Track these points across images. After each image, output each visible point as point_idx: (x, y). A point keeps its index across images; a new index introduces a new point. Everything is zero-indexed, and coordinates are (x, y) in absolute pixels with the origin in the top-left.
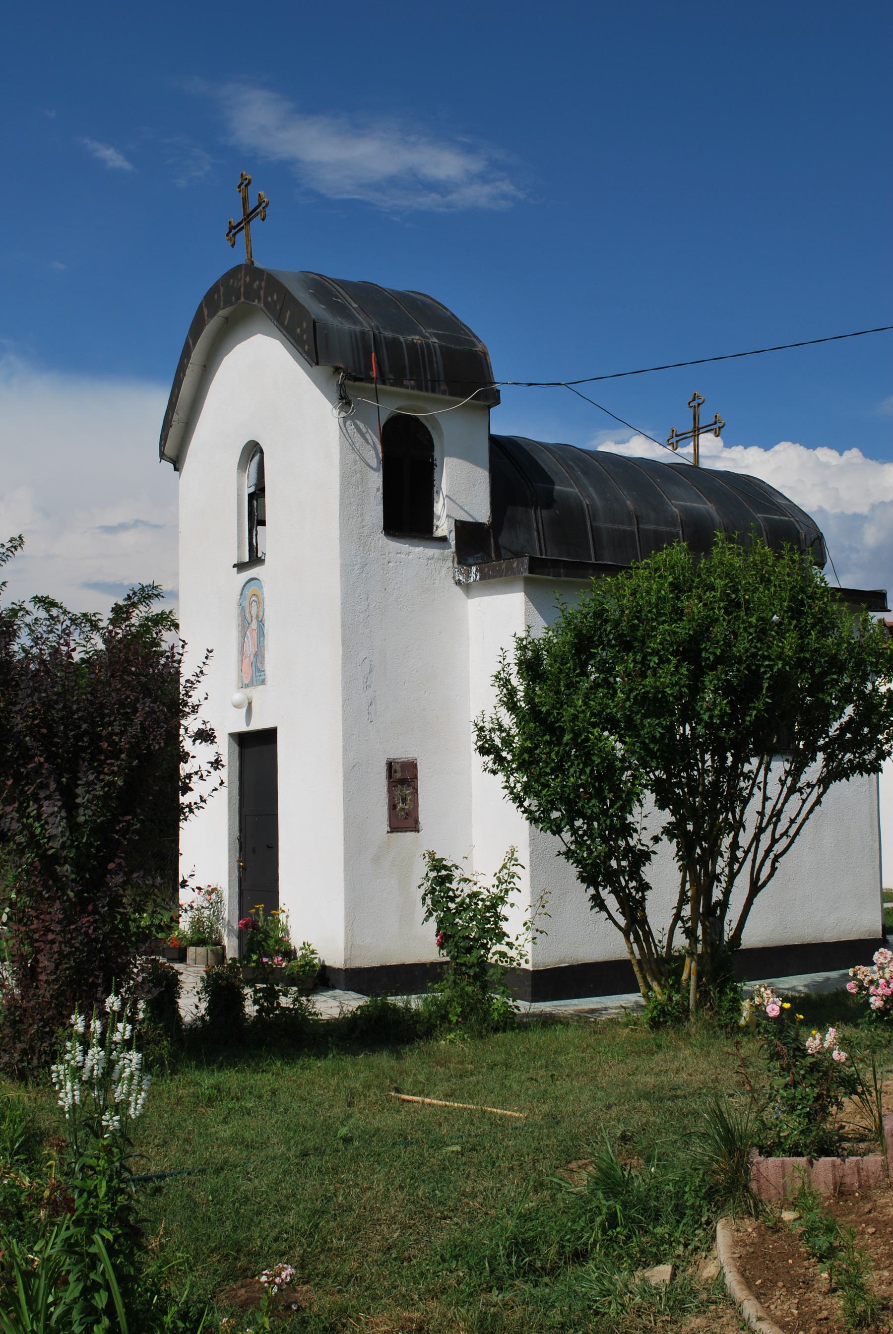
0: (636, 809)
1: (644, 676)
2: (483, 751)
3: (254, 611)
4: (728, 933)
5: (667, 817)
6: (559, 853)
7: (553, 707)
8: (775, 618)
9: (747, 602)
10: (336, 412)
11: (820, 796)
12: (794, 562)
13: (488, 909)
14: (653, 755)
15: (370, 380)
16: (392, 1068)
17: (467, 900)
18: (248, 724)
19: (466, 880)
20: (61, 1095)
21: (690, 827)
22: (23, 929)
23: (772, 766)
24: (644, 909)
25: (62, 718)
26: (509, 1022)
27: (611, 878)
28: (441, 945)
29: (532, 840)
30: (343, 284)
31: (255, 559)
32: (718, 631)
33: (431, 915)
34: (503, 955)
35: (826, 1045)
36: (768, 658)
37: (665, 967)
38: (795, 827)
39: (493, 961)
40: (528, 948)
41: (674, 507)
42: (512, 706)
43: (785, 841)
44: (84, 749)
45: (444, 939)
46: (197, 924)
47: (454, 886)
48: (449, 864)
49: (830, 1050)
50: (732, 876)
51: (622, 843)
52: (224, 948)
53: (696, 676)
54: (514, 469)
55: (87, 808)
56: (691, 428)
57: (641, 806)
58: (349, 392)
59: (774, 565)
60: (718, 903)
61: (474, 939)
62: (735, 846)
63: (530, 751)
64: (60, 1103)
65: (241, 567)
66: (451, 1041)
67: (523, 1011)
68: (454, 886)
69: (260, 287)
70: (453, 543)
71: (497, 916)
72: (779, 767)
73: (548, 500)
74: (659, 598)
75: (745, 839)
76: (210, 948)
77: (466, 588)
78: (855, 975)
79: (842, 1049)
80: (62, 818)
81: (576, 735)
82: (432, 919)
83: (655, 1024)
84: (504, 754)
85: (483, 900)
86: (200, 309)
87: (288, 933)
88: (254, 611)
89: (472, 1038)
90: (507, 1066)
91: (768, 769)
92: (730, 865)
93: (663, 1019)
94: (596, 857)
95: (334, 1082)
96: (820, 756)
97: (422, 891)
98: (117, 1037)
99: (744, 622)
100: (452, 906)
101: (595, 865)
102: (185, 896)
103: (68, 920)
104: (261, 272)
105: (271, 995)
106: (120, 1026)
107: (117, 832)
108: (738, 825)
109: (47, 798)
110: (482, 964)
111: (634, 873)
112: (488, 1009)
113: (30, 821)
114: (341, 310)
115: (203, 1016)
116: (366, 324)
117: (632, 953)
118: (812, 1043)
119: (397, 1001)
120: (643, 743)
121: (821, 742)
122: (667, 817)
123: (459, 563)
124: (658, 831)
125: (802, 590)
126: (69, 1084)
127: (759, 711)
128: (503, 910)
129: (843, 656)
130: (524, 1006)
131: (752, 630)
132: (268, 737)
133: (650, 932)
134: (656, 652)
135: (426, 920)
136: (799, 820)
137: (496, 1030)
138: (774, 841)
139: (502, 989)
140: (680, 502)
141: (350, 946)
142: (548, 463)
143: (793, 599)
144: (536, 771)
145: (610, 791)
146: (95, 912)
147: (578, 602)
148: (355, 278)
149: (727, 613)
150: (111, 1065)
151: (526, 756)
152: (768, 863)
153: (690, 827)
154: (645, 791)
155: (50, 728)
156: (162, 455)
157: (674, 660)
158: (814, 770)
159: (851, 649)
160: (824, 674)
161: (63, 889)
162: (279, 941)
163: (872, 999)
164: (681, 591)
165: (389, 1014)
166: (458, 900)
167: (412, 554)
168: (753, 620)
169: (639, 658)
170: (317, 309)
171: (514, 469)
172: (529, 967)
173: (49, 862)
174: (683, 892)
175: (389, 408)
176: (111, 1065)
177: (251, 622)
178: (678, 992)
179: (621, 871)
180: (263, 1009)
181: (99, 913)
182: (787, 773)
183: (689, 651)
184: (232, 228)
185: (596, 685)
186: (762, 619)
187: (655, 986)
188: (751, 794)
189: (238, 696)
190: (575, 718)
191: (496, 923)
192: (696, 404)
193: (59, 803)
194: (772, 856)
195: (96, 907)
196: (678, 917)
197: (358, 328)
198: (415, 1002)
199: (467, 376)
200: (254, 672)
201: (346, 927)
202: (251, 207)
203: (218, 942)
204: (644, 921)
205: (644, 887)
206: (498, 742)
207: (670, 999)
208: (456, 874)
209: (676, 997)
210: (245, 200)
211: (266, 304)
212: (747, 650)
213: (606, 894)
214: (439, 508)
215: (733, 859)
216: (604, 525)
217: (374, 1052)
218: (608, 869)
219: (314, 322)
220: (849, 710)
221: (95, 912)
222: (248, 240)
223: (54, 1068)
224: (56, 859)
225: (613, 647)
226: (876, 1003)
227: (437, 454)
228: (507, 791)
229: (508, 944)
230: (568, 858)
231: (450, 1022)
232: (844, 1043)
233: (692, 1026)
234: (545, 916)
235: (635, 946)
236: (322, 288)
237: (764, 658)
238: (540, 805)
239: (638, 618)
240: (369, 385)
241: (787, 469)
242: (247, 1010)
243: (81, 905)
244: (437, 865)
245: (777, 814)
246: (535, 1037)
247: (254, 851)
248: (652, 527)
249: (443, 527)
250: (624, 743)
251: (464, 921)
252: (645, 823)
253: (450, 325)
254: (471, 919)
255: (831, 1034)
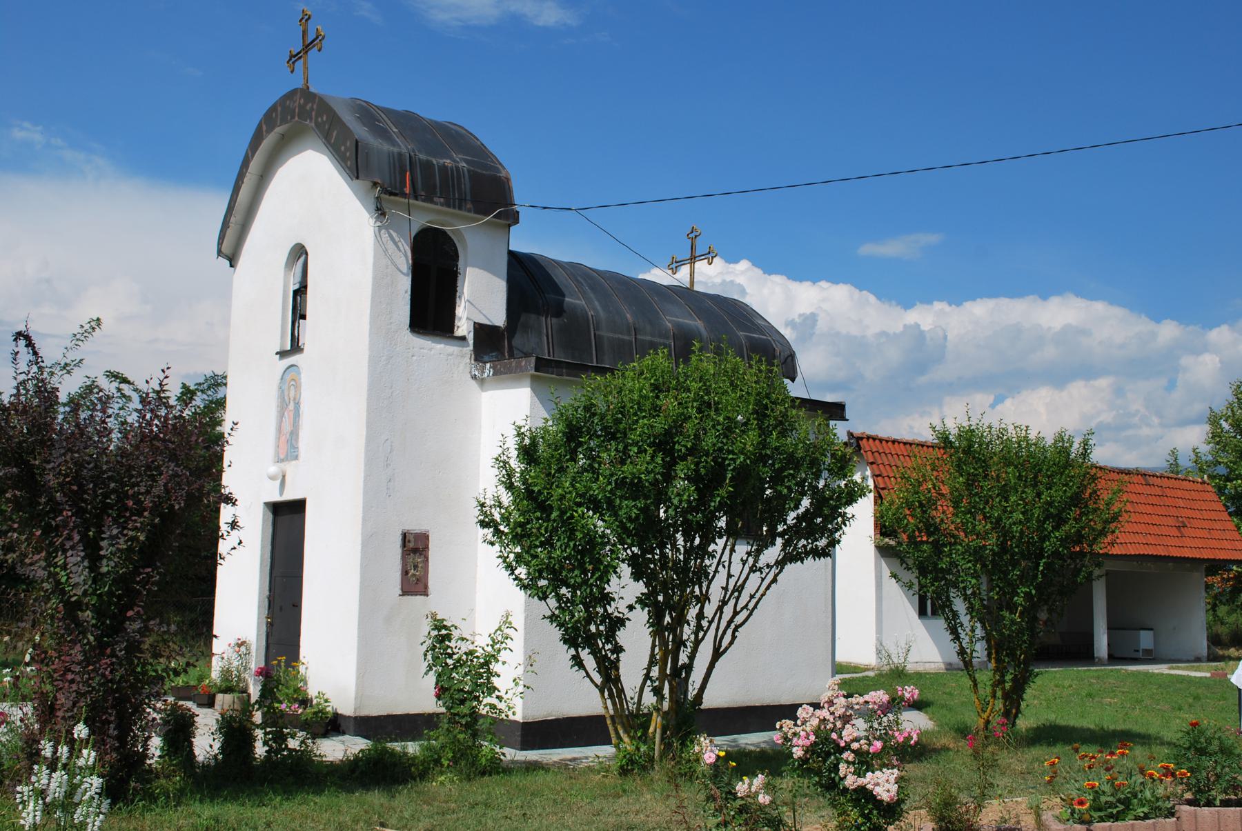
0: (614, 579)
1: (623, 462)
2: (484, 524)
3: (292, 393)
4: (692, 692)
5: (640, 588)
6: (545, 617)
7: (545, 488)
8: (740, 417)
9: (717, 403)
10: (372, 221)
11: (776, 575)
12: (760, 371)
13: (482, 665)
14: (629, 533)
15: (404, 195)
16: (382, 805)
17: (464, 657)
18: (281, 493)
19: (463, 639)
20: (24, 815)
21: (661, 598)
22: (45, 669)
23: (736, 547)
24: (617, 669)
25: (92, 477)
26: (496, 768)
27: (590, 641)
28: (438, 697)
29: (527, 606)
30: (388, 112)
31: (296, 347)
32: (689, 427)
33: (431, 669)
34: (493, 707)
35: (753, 789)
36: (732, 452)
37: (636, 722)
38: (754, 601)
39: (484, 712)
40: (518, 704)
41: (668, 322)
42: (510, 487)
43: (745, 614)
44: (111, 506)
45: (442, 691)
46: (226, 673)
47: (452, 644)
48: (449, 624)
49: (757, 794)
50: (697, 643)
51: (600, 610)
52: (249, 696)
53: (669, 468)
54: (529, 282)
55: (109, 559)
56: (688, 256)
57: (620, 577)
58: (385, 205)
59: (745, 373)
60: (684, 666)
61: (468, 692)
62: (700, 616)
63: (522, 525)
64: (22, 822)
65: (282, 354)
66: (442, 783)
67: (509, 758)
68: (452, 644)
69: (312, 109)
70: (471, 341)
71: (490, 673)
72: (742, 549)
73: (558, 309)
74: (641, 396)
75: (709, 610)
76: (236, 695)
77: (482, 382)
78: (781, 727)
79: (766, 793)
80: (85, 568)
81: (563, 513)
82: (432, 673)
83: (624, 772)
84: (502, 528)
85: (478, 657)
86: (260, 123)
87: (306, 683)
88: (292, 393)
89: (461, 781)
90: (487, 805)
91: (732, 550)
92: (696, 633)
93: (629, 767)
94: (577, 622)
95: (326, 816)
96: (779, 541)
97: (424, 647)
98: (81, 762)
99: (713, 420)
100: (450, 662)
101: (575, 628)
102: (218, 646)
103: (87, 661)
104: (314, 96)
105: (280, 738)
106: (85, 752)
107: (138, 583)
108: (704, 599)
109: (72, 548)
110: (475, 716)
111: (610, 636)
112: (477, 756)
113: (58, 570)
114: (383, 133)
115: (216, 756)
116: (404, 147)
117: (606, 708)
118: (741, 788)
119: (397, 746)
120: (621, 522)
121: (780, 528)
122: (640, 588)
123: (476, 360)
124: (632, 601)
125: (768, 396)
126: (32, 804)
127: (722, 498)
128: (495, 667)
129: (800, 454)
130: (511, 754)
131: (719, 428)
132: (298, 507)
133: (623, 690)
134: (636, 443)
135: (426, 674)
136: (758, 595)
137: (483, 774)
138: (736, 613)
139: (490, 737)
140: (674, 318)
141: (359, 696)
142: (560, 277)
143: (758, 402)
144: (526, 542)
145: (590, 563)
146: (113, 655)
147: (572, 396)
148: (399, 107)
149: (699, 411)
150: (72, 790)
151: (519, 530)
152: (730, 632)
153: (661, 598)
154: (622, 565)
155: (81, 486)
156: (220, 253)
157: (650, 451)
158: (772, 554)
159: (807, 448)
160: (782, 469)
161: (84, 633)
162: (297, 690)
163: (794, 750)
164: (661, 391)
165: (389, 757)
166: (455, 657)
167: (432, 349)
168: (721, 419)
169: (621, 447)
170: (360, 131)
171: (529, 282)
172: (519, 717)
173: (73, 608)
174: (652, 655)
175: (420, 220)
176: (72, 790)
177: (289, 405)
178: (645, 743)
179: (599, 634)
180: (273, 749)
181: (117, 656)
182: (749, 554)
183: (663, 443)
184: (292, 56)
185: (584, 470)
186: (728, 418)
187: (626, 739)
188: (716, 571)
189: (273, 469)
190: (562, 498)
191: (488, 678)
192: (693, 235)
193: (82, 554)
194: (733, 626)
195: (113, 651)
196: (647, 677)
197: (396, 150)
198: (413, 748)
199: (491, 197)
200: (288, 448)
201: (358, 678)
202: (310, 38)
203: (245, 691)
204: (618, 679)
205: (618, 649)
206: (497, 517)
207: (638, 749)
208: (455, 634)
209: (643, 748)
210: (304, 33)
211: (317, 124)
212: (714, 445)
213: (585, 655)
214: (462, 311)
215: (699, 627)
216: (605, 334)
217: (368, 790)
218: (588, 632)
219: (357, 142)
220: (806, 503)
221: (113, 655)
222: (306, 68)
223: (19, 789)
224: (79, 605)
225: (599, 437)
226: (798, 752)
227: (461, 263)
228: (500, 560)
229: (498, 697)
230: (552, 622)
231: (442, 766)
232: (769, 787)
233: (657, 774)
234: (532, 674)
235: (609, 702)
236: (367, 113)
237: (729, 452)
238: (529, 574)
239: (622, 413)
240: (403, 200)
241: (776, 299)
242: (257, 750)
243: (101, 646)
244: (439, 625)
245: (739, 589)
246: (528, 781)
247: (281, 609)
248: (648, 338)
249: (463, 327)
250: (603, 520)
251: (461, 676)
252: (622, 593)
253: (478, 152)
254: (466, 674)
255: (759, 780)
